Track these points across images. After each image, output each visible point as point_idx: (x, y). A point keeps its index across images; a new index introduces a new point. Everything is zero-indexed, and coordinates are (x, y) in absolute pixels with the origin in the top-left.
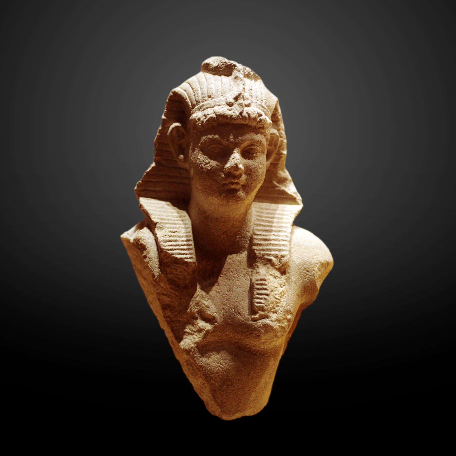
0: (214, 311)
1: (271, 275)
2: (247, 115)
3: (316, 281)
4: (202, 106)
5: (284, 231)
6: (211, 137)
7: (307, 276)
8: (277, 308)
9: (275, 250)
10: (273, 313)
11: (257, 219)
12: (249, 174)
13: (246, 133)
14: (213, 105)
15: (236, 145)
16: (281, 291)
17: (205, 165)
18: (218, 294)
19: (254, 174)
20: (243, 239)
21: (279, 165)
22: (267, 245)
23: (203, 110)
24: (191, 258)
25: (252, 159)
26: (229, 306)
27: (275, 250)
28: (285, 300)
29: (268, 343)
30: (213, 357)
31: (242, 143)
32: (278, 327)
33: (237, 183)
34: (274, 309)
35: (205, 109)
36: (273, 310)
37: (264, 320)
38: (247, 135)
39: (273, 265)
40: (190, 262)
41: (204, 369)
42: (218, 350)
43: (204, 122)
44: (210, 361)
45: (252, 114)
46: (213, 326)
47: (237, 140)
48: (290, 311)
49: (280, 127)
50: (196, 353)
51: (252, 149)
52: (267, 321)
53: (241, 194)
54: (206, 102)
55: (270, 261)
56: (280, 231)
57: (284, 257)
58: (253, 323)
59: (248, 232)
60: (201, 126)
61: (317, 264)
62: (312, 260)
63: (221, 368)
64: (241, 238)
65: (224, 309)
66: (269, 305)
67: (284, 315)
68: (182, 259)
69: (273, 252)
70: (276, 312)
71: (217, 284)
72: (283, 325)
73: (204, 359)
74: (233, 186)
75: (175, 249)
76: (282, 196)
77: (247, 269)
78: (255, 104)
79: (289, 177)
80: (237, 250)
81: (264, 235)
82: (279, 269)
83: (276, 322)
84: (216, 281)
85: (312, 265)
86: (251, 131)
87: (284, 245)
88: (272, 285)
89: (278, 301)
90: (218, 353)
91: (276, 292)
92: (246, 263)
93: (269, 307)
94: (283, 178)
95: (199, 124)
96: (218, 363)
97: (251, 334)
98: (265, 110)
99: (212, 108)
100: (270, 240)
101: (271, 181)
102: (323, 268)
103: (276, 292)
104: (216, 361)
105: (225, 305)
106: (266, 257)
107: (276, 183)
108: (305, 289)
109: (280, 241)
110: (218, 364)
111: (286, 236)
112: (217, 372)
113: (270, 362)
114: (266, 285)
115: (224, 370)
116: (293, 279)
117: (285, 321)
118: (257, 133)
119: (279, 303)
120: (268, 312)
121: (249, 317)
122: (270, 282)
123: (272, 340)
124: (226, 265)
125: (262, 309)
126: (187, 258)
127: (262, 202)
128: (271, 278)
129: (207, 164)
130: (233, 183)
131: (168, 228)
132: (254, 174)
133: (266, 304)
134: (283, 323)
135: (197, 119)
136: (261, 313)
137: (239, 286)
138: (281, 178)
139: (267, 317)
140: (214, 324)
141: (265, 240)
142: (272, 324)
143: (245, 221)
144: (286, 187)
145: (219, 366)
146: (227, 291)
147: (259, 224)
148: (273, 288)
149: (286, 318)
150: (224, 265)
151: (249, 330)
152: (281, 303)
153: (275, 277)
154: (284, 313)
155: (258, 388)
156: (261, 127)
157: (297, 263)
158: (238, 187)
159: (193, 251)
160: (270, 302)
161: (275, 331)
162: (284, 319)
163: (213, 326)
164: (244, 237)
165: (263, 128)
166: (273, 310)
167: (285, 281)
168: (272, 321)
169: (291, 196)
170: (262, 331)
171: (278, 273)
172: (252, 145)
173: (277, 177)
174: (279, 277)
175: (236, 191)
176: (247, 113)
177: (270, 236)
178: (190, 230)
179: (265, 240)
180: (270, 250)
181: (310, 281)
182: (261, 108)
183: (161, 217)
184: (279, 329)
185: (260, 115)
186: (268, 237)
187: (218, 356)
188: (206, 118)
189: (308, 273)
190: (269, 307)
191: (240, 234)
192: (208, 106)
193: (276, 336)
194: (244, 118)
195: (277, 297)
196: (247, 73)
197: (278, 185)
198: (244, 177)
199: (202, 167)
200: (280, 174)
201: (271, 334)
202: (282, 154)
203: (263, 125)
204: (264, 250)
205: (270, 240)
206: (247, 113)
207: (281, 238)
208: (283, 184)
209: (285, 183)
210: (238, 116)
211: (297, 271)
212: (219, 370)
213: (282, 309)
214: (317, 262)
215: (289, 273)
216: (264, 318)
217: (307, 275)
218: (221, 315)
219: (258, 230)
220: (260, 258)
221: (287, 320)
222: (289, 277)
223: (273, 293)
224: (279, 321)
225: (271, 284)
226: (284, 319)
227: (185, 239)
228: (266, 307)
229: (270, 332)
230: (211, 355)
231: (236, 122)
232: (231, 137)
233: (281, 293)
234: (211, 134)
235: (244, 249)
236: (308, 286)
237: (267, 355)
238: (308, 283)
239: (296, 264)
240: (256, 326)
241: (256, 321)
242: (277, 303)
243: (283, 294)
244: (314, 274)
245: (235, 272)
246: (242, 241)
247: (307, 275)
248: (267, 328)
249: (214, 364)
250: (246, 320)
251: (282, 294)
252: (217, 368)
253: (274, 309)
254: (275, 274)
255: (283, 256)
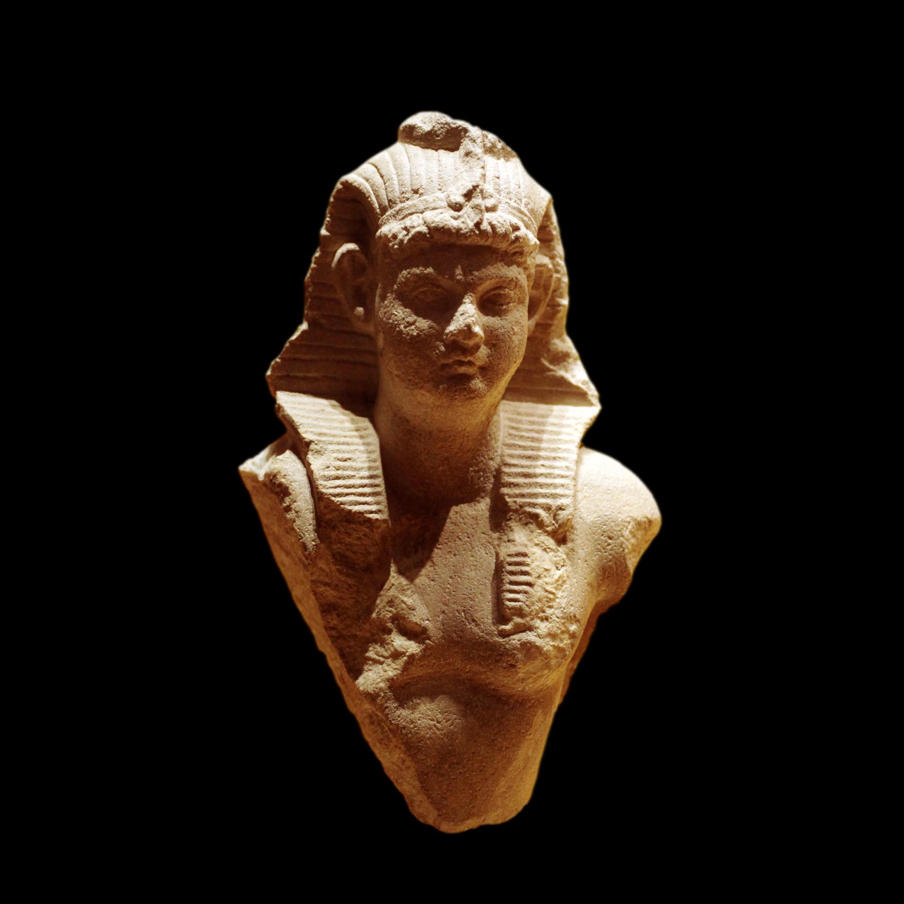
0: (425, 617)
1: (537, 545)
2: (489, 229)
3: (627, 556)
4: (400, 210)
5: (564, 459)
6: (418, 272)
7: (609, 547)
8: (549, 612)
9: (545, 496)
10: (542, 620)
11: (510, 435)
12: (494, 345)
13: (489, 264)
14: (422, 207)
15: (469, 287)
16: (556, 577)
17: (405, 327)
18: (432, 583)
19: (503, 345)
20: (481, 473)
21: (553, 328)
22: (530, 485)
23: (403, 218)
24: (378, 512)
25: (500, 316)
26: (455, 606)
27: (545, 496)
28: (566, 594)
29: (530, 680)
30: (422, 708)
31: (481, 284)
32: (551, 648)
33: (470, 363)
34: (544, 612)
35: (406, 216)
36: (541, 614)
37: (524, 634)
38: (489, 267)
39: (541, 525)
40: (377, 519)
41: (404, 732)
42: (432, 694)
43: (405, 242)
44: (417, 715)
45: (499, 225)
46: (422, 647)
47: (470, 277)
48: (575, 616)
49: (556, 253)
50: (389, 699)
51: (500, 294)
52: (530, 636)
53: (478, 384)
54: (409, 203)
55: (535, 517)
56: (554, 458)
57: (563, 510)
58: (501, 640)
59: (492, 459)
60: (398, 249)
61: (629, 522)
62: (619, 515)
63: (438, 729)
64: (478, 471)
65: (444, 612)
66: (533, 604)
67: (563, 623)
68: (361, 513)
69: (541, 501)
70: (547, 619)
71: (429, 563)
72: (561, 645)
73: (404, 712)
74: (462, 370)
75: (347, 494)
76: (560, 389)
77: (490, 532)
78: (506, 206)
79: (574, 351)
80: (470, 496)
81: (522, 467)
82: (553, 534)
83: (548, 639)
84: (429, 557)
85: (618, 525)
86: (497, 260)
87: (563, 486)
88: (538, 566)
89: (552, 596)
90: (433, 700)
91: (547, 580)
92: (487, 520)
93: (533, 608)
94: (562, 352)
95: (394, 245)
96: (432, 720)
97: (497, 661)
98: (525, 218)
99: (420, 215)
100: (535, 476)
101: (537, 360)
102: (640, 532)
103: (547, 580)
104: (428, 715)
105: (446, 605)
106: (528, 509)
107: (547, 364)
108: (604, 573)
109: (555, 478)
110: (432, 723)
111: (567, 468)
112: (430, 738)
113: (536, 718)
114: (528, 565)
115: (445, 734)
116: (582, 553)
117: (566, 636)
118: (509, 264)
119: (553, 600)
120: (532, 619)
121: (493, 628)
122: (536, 559)
123: (539, 674)
125: (520, 613)
126: (371, 512)
127: (520, 400)
128: (538, 551)
129: (410, 324)
130: (461, 363)
131: (333, 451)
132: (503, 345)
133: (527, 603)
134: (562, 640)
135: (390, 236)
136: (518, 620)
137: (473, 568)
138: (558, 353)
139: (530, 629)
140: (424, 643)
141: (526, 476)
142: (539, 642)
143: (485, 438)
144: (567, 371)
145: (435, 726)
146: (451, 577)
147: (514, 445)
148: (541, 571)
149: (567, 631)
150: (443, 525)
151: (494, 655)
152: (558, 600)
153: (545, 550)
154: (563, 621)
155: (511, 769)
156: (516, 252)
157: (588, 521)
158: (471, 370)
159: (383, 498)
160: (536, 598)
161: (546, 656)
162: (563, 632)
163: (422, 647)
164: (484, 471)
165: (521, 253)
166: (541, 614)
167: (564, 556)
168: (539, 636)
169: (578, 388)
170: (520, 656)
171: (550, 542)
172: (500, 287)
173: (549, 350)
174: (552, 550)
175: (468, 378)
176: (490, 224)
177: (535, 467)
178: (377, 455)
179: (526, 476)
180: (535, 495)
181: (614, 557)
182: (517, 214)
183: (318, 431)
184: (553, 653)
185: (516, 228)
186: (531, 471)
187: (433, 706)
188: (407, 235)
189: (610, 541)
190: (533, 608)
191: (476, 465)
192: (413, 210)
193: (547, 666)
194: (483, 233)
195: (549, 588)
196: (489, 145)
197: (551, 367)
198: (484, 351)
199: (401, 332)
200: (554, 344)
201: (538, 663)
203: (521, 247)
204: (523, 496)
205: (535, 476)
206: (490, 224)
207: (557, 472)
208: (561, 365)
209: (565, 363)
210: (472, 230)
211: (589, 537)
212: (434, 733)
213: (558, 613)
214: (628, 519)
215: (573, 541)
216: (524, 631)
217: (609, 545)
218: (439, 625)
219: (511, 456)
220: (516, 511)
221: (570, 635)
222: (573, 550)
223: (540, 581)
224: (553, 636)
225: (538, 563)
226: (563, 632)
227: (366, 473)
228: (527, 609)
229: (536, 658)
230: (419, 704)
231: (469, 241)
232: (459, 271)
233: (557, 581)
234: (417, 267)
235: (483, 494)
236: (610, 567)
237: (529, 704)
238: (611, 561)
239: (587, 524)
240: (507, 646)
241: (508, 636)
242: (550, 601)
243: (560, 583)
244: (622, 543)
245: (467, 539)
246: (479, 479)
247: (609, 545)
248: (530, 649)
249: (424, 722)
250: (487, 634)
251: (560, 582)
252: (430, 729)
253: (544, 612)
254: (546, 543)
255: (561, 508)
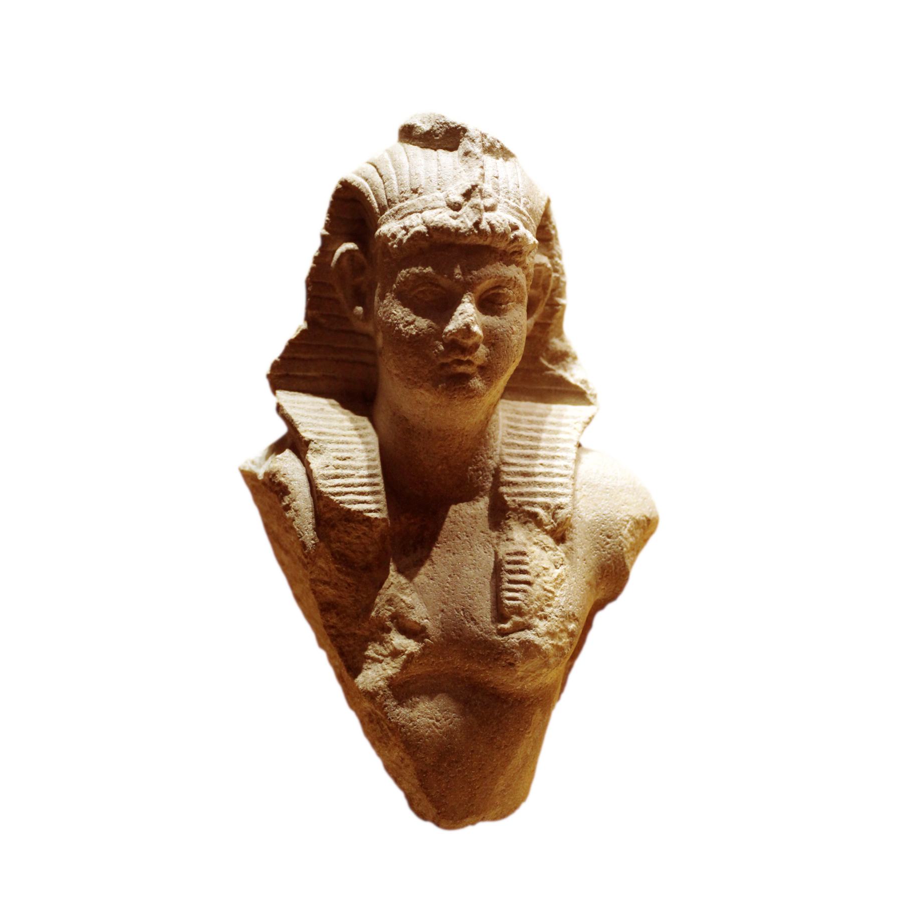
0: (424, 616)
1: (535, 544)
2: (488, 228)
3: (626, 555)
4: (400, 209)
5: (563, 458)
6: (417, 271)
7: (608, 546)
8: (548, 610)
9: (543, 495)
10: (541, 618)
11: (509, 434)
12: (493, 345)
13: (487, 263)
14: (421, 207)
15: (468, 287)
16: (555, 576)
17: (405, 326)
18: (431, 582)
19: (502, 344)
20: (480, 472)
21: (552, 327)
22: (529, 484)
23: (402, 218)
24: (377, 511)
25: (499, 315)
26: (454, 605)
27: (543, 495)
28: (564, 593)
29: (529, 679)
30: (422, 706)
31: (480, 283)
32: (550, 647)
33: (469, 363)
34: (542, 610)
35: (405, 216)
36: (540, 613)
37: (522, 633)
38: (488, 266)
39: (539, 524)
40: (376, 518)
41: (403, 730)
42: (431, 692)
43: (404, 241)
44: (416, 713)
45: (498, 225)
46: (422, 645)
47: (469, 277)
48: (574, 615)
49: (554, 252)
50: (388, 698)
51: (499, 294)
52: (528, 635)
53: (477, 383)
54: (408, 202)
55: (534, 516)
56: (553, 457)
57: (562, 508)
58: (500, 639)
59: (491, 458)
60: (397, 248)
61: (628, 521)
62: (618, 514)
63: (437, 727)
64: (477, 470)
65: (443, 611)
66: (532, 603)
67: (562, 622)
68: (360, 512)
69: (540, 499)
70: (545, 617)
71: (428, 562)
72: (560, 644)
73: (404, 711)
74: (461, 369)
75: (346, 493)
76: (559, 388)
77: (489, 531)
78: (505, 205)
80: (469, 494)
81: (521, 466)
82: (551, 533)
83: (547, 638)
84: (428, 556)
85: (616, 524)
86: (496, 260)
87: (562, 485)
88: (537, 565)
89: (550, 595)
90: (432, 699)
91: (545, 578)
92: (486, 519)
93: (532, 606)
94: (561, 351)
95: (393, 245)
96: (431, 718)
97: (496, 660)
98: (524, 218)
100: (533, 475)
101: (536, 359)
102: (638, 531)
103: (545, 578)
104: (427, 714)
105: (445, 603)
106: (527, 508)
107: (545, 363)
108: (603, 572)
109: (553, 477)
110: (431, 721)
111: (566, 466)
112: (429, 736)
113: (534, 717)
114: (527, 564)
115: (444, 733)
116: (580, 552)
117: (565, 635)
118: (508, 264)
119: (552, 599)
120: (531, 618)
121: (492, 627)
122: (535, 558)
123: (538, 672)
124: (447, 525)
125: (519, 611)
126: (371, 511)
127: (519, 399)
128: (536, 550)
129: (409, 323)
130: (460, 363)
131: (332, 450)
132: (502, 344)
133: (526, 601)
134: (560, 639)
135: (389, 236)
136: (517, 618)
137: (472, 566)
138: (556, 352)
139: (529, 627)
140: (423, 642)
141: (525, 474)
142: (538, 641)
143: (484, 437)
144: (565, 370)
145: (434, 724)
146: (450, 576)
147: (513, 444)
148: (539, 569)
149: (566, 630)
150: (442, 523)
151: (493, 653)
152: (556, 599)
153: (544, 549)
154: (562, 619)
155: (509, 767)
156: (515, 252)
157: (587, 520)
158: (470, 370)
159: (382, 497)
160: (534, 597)
161: (544, 654)
162: (561, 631)
163: (422, 645)
164: (483, 470)
165: (520, 253)
166: (540, 613)
167: (563, 555)
168: (537, 634)
169: (576, 387)
170: (518, 654)
171: (549, 541)
172: (499, 287)
173: (548, 349)
174: (551, 549)
175: (467, 377)
176: (489, 223)
177: (534, 466)
178: (376, 454)
179: (525, 474)
180: (534, 494)
181: (613, 556)
182: (516, 213)
183: (318, 430)
184: (552, 651)
185: (515, 228)
186: (530, 470)
187: (432, 704)
188: (407, 234)
189: (609, 540)
190: (532, 606)
191: (475, 464)
192: (412, 210)
193: (546, 665)
194: (482, 233)
195: (548, 587)
196: (488, 144)
197: (550, 366)
198: (482, 350)
199: (400, 331)
200: (553, 343)
201: (537, 661)
202: (558, 305)
203: (520, 246)
204: (522, 495)
205: (533, 475)
206: (489, 223)
207: (555, 471)
208: (560, 364)
209: (564, 363)
210: (471, 230)
211: (588, 536)
212: (433, 731)
213: (557, 611)
214: (627, 518)
215: (571, 539)
216: (523, 630)
217: (608, 543)
218: (438, 623)
219: (510, 455)
220: (515, 510)
221: (569, 633)
222: (572, 549)
223: (539, 580)
224: (552, 634)
225: (536, 562)
226: (561, 631)
227: (365, 472)
228: (526, 608)
229: (535, 656)
230: (418, 703)
231: (468, 241)
232: (457, 271)
233: (556, 579)
234: (417, 266)
235: (482, 493)
236: (609, 566)
237: (528, 703)
238: (609, 559)
239: (585, 523)
240: (506, 645)
241: (507, 634)
242: (548, 599)
243: (559, 581)
244: (621, 542)
245: (465, 538)
246: (478, 478)
247: (608, 543)
248: (528, 648)
249: (423, 721)
250: (486, 633)
251: (559, 581)
252: (429, 727)
253: (542, 610)
254: (545, 541)
255: (559, 507)
